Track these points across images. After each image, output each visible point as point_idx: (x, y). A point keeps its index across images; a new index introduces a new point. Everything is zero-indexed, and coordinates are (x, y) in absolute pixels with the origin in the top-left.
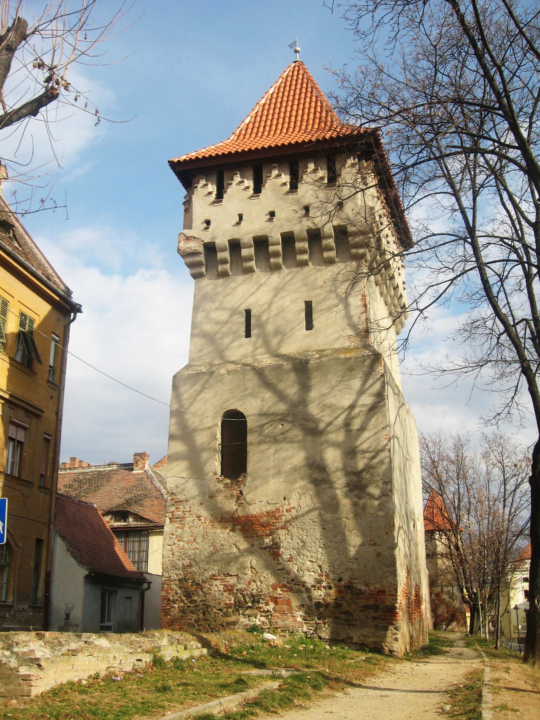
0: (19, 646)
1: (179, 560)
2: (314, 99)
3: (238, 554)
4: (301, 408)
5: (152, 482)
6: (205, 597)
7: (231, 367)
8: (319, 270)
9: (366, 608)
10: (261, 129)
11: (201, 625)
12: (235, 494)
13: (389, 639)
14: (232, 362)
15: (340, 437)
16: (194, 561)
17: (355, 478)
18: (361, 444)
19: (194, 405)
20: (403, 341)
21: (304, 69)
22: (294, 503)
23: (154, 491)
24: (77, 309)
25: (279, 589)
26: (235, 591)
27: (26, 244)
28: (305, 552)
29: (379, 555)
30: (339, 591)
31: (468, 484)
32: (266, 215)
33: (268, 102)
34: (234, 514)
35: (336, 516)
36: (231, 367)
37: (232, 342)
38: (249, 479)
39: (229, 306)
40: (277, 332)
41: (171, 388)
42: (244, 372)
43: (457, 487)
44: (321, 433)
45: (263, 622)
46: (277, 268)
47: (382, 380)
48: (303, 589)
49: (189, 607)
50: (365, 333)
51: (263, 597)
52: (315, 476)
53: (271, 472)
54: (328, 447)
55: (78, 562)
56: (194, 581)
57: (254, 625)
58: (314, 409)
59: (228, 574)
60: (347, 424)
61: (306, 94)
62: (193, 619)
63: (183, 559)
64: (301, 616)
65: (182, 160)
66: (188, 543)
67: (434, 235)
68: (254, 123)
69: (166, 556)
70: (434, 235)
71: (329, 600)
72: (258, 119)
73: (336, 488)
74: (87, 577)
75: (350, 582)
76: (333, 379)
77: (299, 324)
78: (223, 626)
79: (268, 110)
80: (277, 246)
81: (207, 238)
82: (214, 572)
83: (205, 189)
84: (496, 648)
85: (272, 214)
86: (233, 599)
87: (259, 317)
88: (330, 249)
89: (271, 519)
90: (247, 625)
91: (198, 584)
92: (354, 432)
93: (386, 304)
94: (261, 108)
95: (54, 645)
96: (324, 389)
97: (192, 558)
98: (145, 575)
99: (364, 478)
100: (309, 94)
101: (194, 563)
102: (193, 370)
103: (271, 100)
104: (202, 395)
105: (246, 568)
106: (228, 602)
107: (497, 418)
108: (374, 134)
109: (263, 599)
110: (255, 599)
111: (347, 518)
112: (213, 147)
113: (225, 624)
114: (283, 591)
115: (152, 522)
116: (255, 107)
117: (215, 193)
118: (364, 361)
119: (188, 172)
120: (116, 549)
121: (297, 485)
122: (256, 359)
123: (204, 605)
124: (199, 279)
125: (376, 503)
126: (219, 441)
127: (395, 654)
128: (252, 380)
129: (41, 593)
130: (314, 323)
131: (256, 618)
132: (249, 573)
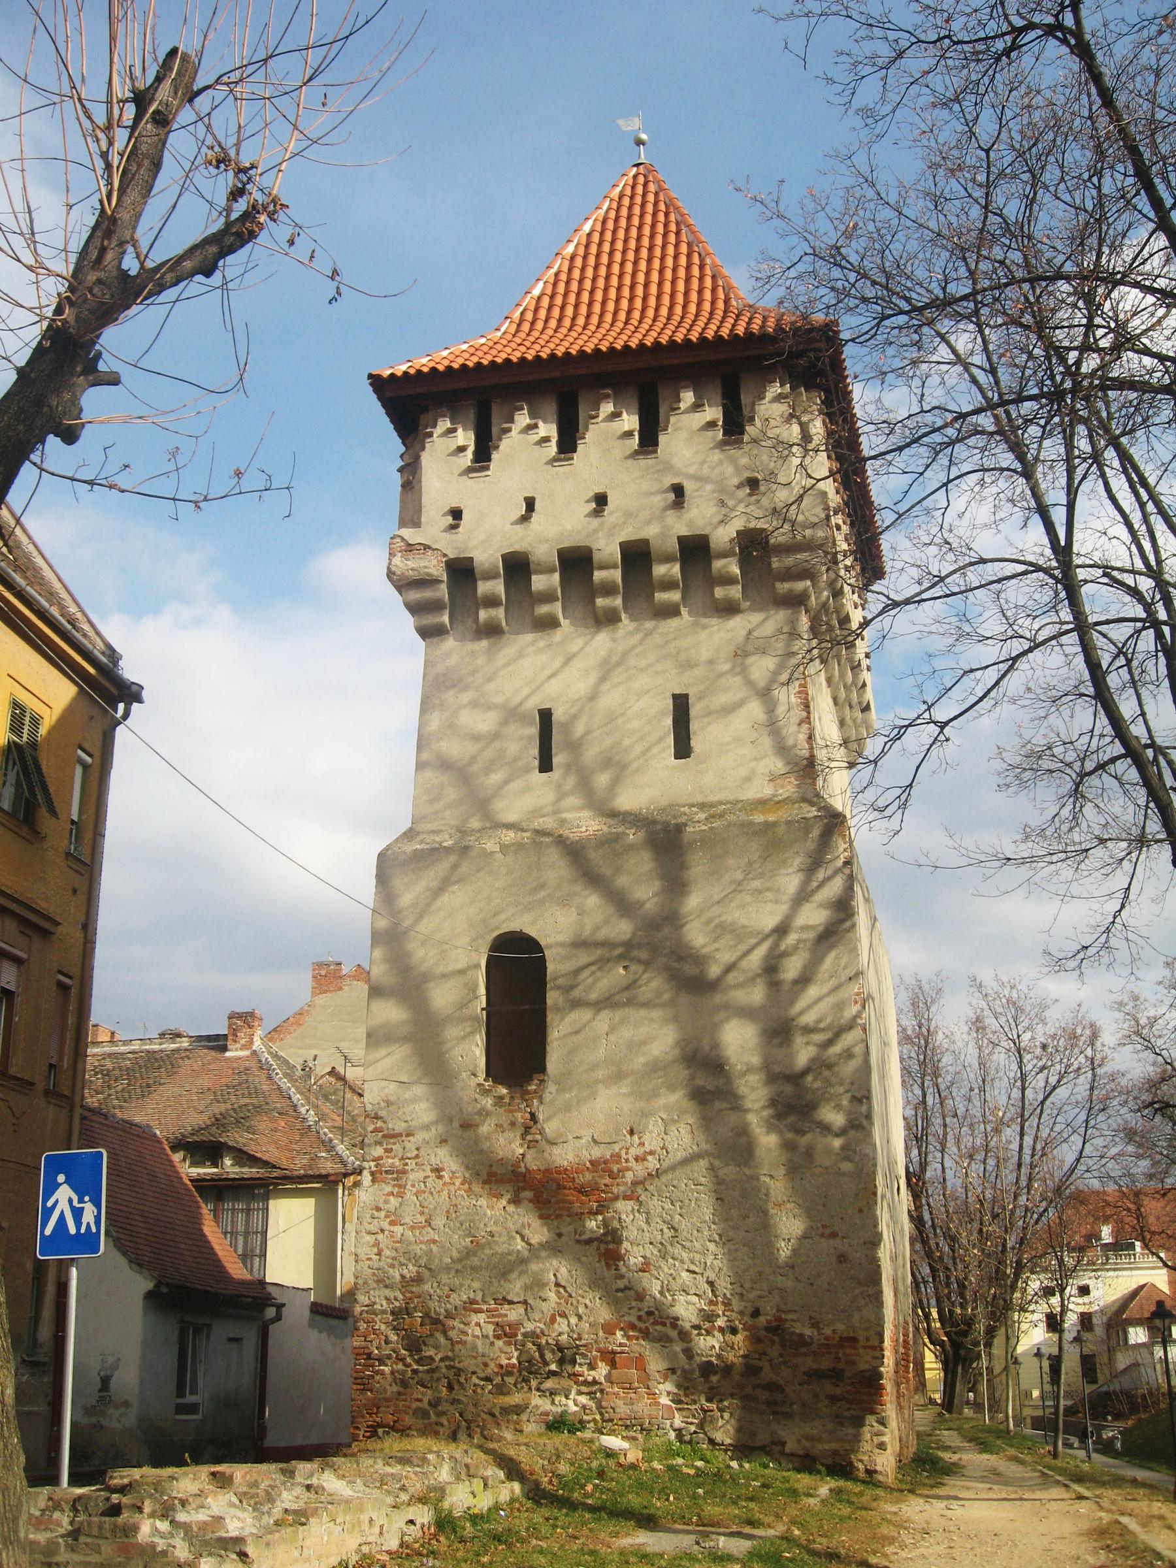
0: (188, 1507)
1: (392, 1266)
2: (684, 248)
3: (526, 1253)
4: (666, 930)
5: (270, 1078)
6: (452, 1350)
7: (509, 836)
8: (705, 627)
9: (814, 1375)
10: (570, 311)
11: (443, 1413)
12: (521, 1120)
13: (866, 1446)
14: (509, 826)
15: (756, 995)
16: (427, 1270)
17: (789, 1089)
18: (801, 1013)
19: (426, 920)
20: (900, 791)
21: (657, 181)
22: (652, 1141)
23: (275, 1096)
24: (131, 694)
25: (619, 1334)
26: (520, 1337)
27: (19, 545)
28: (677, 1250)
29: (842, 1258)
30: (755, 1339)
31: (942, 1087)
32: (588, 501)
33: (581, 251)
34: (516, 1165)
35: (747, 1171)
36: (509, 836)
37: (507, 782)
38: (551, 1087)
39: (499, 699)
40: (607, 762)
41: (373, 882)
42: (537, 846)
43: (918, 1092)
44: (712, 986)
45: (584, 1407)
46: (610, 619)
47: (847, 871)
48: (673, 1334)
49: (415, 1372)
50: (808, 769)
51: (582, 1350)
52: (699, 1082)
53: (600, 1073)
54: (727, 1019)
55: (130, 1261)
56: (427, 1315)
57: (563, 1414)
58: (696, 936)
59: (504, 1299)
60: (771, 968)
61: (665, 235)
62: (426, 1400)
63: (401, 1264)
64: (668, 1393)
65: (399, 374)
66: (412, 1228)
67: (983, 561)
68: (552, 297)
69: (362, 1256)
70: (983, 561)
71: (731, 1357)
72: (561, 288)
73: (747, 1111)
74: (150, 1296)
75: (779, 1319)
76: (734, 867)
77: (660, 741)
78: (493, 1415)
79: (583, 270)
80: (612, 571)
81: (450, 545)
82: (472, 1295)
83: (449, 441)
84: (1055, 1455)
85: (601, 500)
86: (516, 1354)
87: (567, 726)
88: (729, 581)
89: (602, 1177)
90: (547, 1414)
91: (436, 1322)
92: (786, 987)
93: (836, 703)
94: (567, 263)
95: (256, 1500)
96: (717, 892)
97: (422, 1262)
98: (270, 1289)
99: (807, 1089)
100: (672, 238)
101: (426, 1274)
102: (422, 842)
103: (587, 246)
104: (445, 898)
105: (546, 1285)
106: (504, 1362)
107: (1081, 955)
108: (828, 335)
109: (583, 1355)
110: (567, 1355)
111: (771, 1177)
112: (464, 347)
113: (497, 1412)
114: (629, 1338)
115: (274, 1167)
116: (553, 262)
117: (471, 449)
118: (807, 831)
119: (412, 402)
120: (207, 1230)
121: (660, 1102)
122: (563, 822)
123: (449, 1368)
124: (436, 640)
125: (837, 1143)
126: (483, 1002)
127: (880, 1478)
128: (556, 868)
129: (45, 1332)
130: (693, 743)
131: (567, 1397)
132: (552, 1295)
